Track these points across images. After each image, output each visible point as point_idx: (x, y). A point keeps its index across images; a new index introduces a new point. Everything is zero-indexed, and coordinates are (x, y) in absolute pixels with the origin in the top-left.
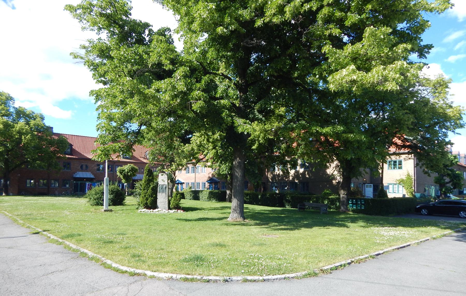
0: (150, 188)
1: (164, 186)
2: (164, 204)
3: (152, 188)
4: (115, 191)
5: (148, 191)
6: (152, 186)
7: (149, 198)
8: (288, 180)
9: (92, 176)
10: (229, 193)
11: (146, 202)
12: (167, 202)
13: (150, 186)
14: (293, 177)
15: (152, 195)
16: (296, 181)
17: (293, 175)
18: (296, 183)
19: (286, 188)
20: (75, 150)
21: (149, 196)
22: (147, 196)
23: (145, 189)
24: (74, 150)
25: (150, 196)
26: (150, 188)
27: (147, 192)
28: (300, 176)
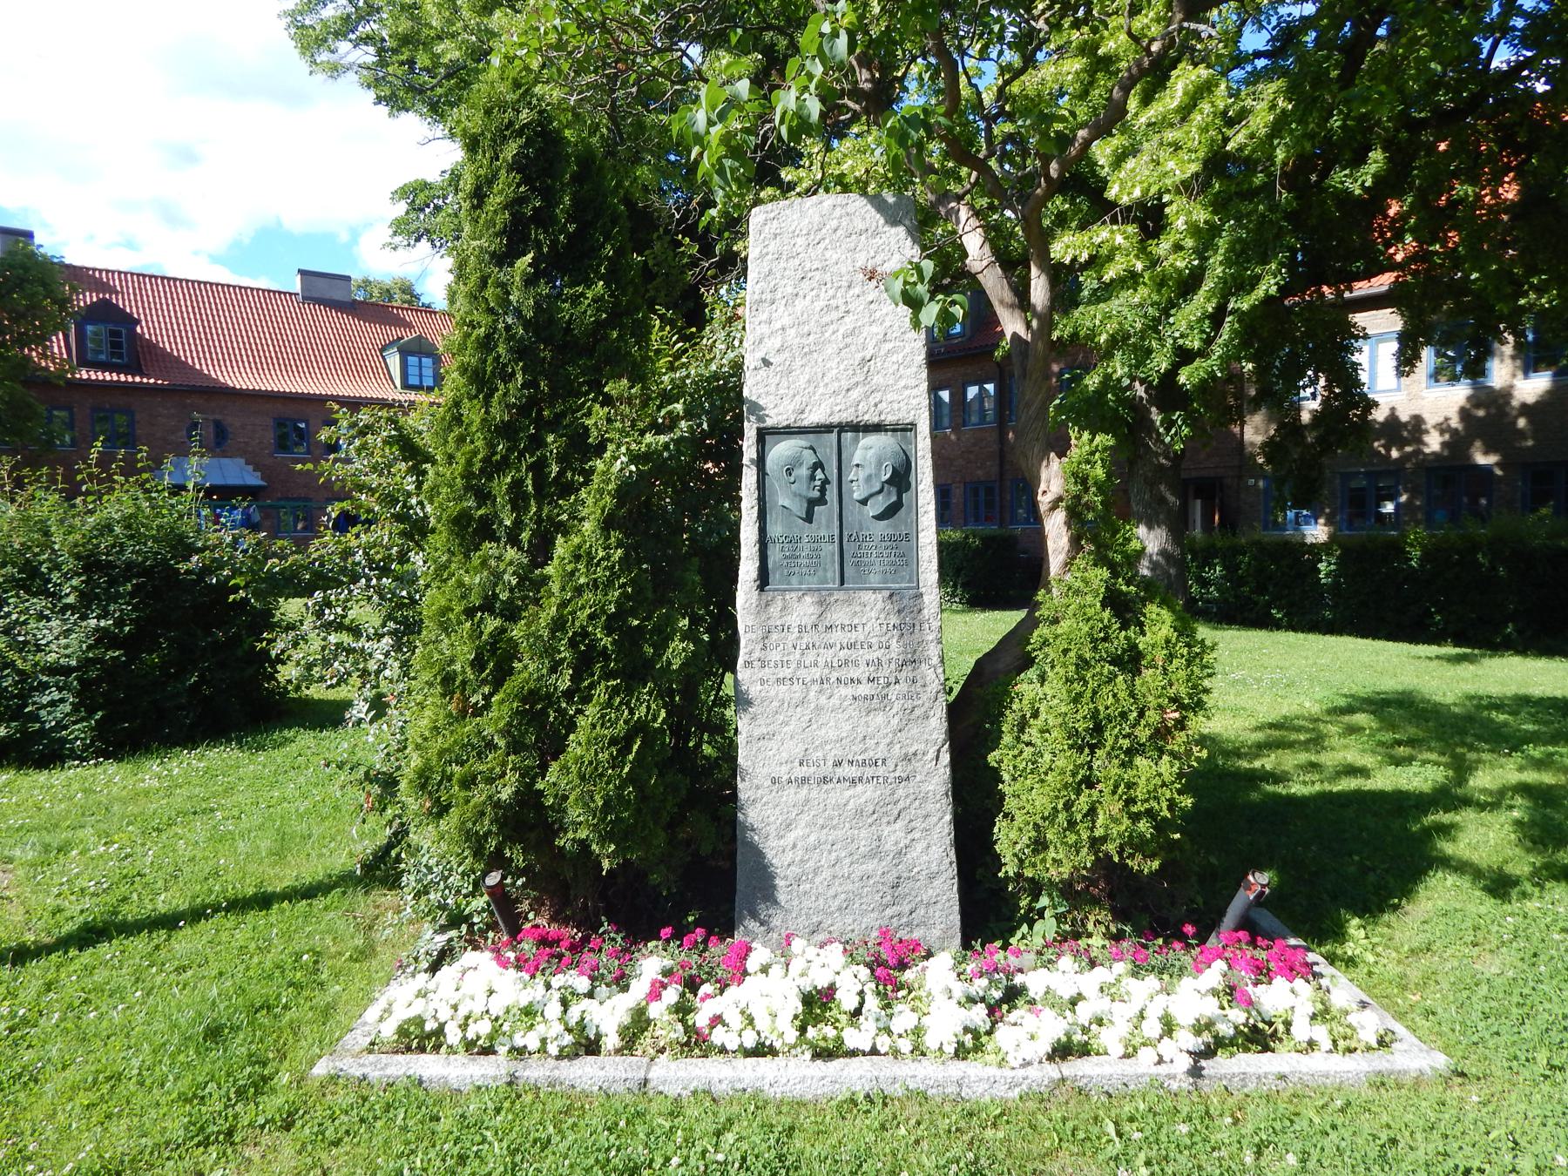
0: (592, 504)
1: (869, 452)
2: (889, 812)
3: (625, 492)
4: (130, 569)
5: (541, 551)
6: (613, 466)
7: (579, 694)
8: (1405, 458)
9: (254, 479)
10: (1163, 552)
11: (528, 797)
12: (936, 777)
13: (582, 449)
14: (1454, 432)
15: (627, 641)
16: (1482, 459)
17: (1455, 423)
18: (1487, 470)
19: (1389, 508)
20: (156, 346)
21: (582, 666)
22: (528, 668)
23: (486, 530)
24: (151, 347)
25: (585, 660)
26: (592, 504)
27: (532, 584)
28: (1522, 423)
